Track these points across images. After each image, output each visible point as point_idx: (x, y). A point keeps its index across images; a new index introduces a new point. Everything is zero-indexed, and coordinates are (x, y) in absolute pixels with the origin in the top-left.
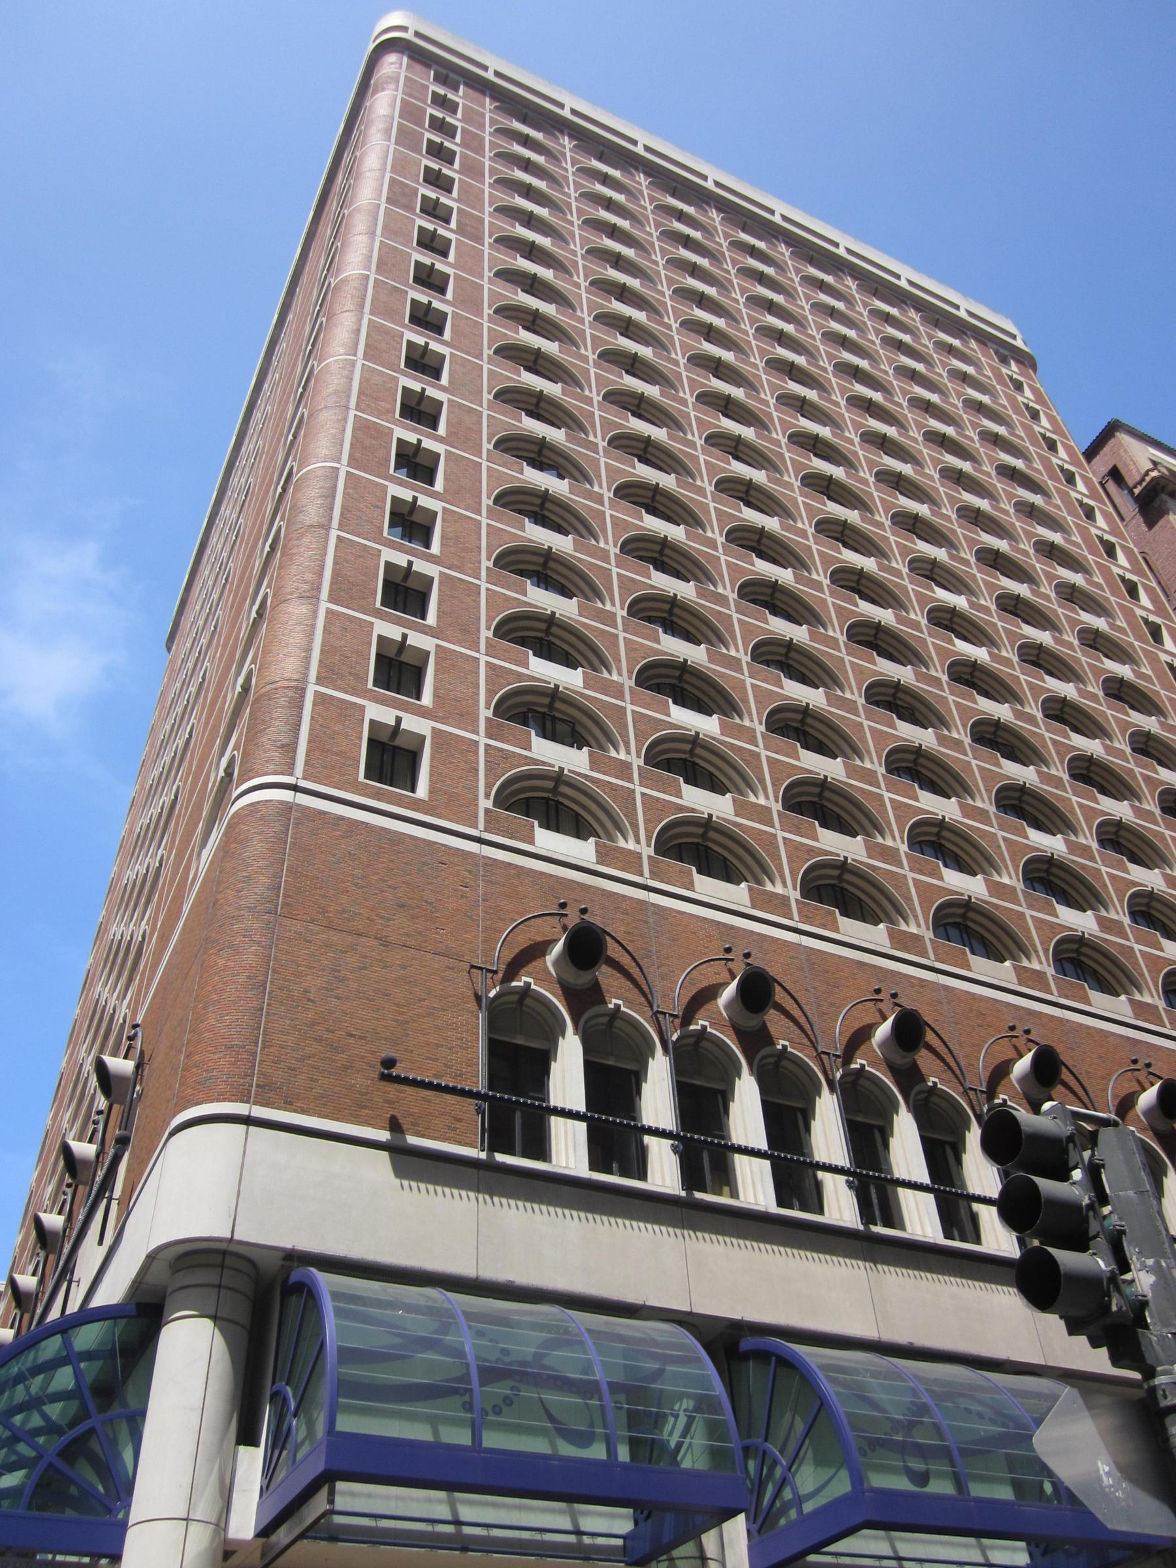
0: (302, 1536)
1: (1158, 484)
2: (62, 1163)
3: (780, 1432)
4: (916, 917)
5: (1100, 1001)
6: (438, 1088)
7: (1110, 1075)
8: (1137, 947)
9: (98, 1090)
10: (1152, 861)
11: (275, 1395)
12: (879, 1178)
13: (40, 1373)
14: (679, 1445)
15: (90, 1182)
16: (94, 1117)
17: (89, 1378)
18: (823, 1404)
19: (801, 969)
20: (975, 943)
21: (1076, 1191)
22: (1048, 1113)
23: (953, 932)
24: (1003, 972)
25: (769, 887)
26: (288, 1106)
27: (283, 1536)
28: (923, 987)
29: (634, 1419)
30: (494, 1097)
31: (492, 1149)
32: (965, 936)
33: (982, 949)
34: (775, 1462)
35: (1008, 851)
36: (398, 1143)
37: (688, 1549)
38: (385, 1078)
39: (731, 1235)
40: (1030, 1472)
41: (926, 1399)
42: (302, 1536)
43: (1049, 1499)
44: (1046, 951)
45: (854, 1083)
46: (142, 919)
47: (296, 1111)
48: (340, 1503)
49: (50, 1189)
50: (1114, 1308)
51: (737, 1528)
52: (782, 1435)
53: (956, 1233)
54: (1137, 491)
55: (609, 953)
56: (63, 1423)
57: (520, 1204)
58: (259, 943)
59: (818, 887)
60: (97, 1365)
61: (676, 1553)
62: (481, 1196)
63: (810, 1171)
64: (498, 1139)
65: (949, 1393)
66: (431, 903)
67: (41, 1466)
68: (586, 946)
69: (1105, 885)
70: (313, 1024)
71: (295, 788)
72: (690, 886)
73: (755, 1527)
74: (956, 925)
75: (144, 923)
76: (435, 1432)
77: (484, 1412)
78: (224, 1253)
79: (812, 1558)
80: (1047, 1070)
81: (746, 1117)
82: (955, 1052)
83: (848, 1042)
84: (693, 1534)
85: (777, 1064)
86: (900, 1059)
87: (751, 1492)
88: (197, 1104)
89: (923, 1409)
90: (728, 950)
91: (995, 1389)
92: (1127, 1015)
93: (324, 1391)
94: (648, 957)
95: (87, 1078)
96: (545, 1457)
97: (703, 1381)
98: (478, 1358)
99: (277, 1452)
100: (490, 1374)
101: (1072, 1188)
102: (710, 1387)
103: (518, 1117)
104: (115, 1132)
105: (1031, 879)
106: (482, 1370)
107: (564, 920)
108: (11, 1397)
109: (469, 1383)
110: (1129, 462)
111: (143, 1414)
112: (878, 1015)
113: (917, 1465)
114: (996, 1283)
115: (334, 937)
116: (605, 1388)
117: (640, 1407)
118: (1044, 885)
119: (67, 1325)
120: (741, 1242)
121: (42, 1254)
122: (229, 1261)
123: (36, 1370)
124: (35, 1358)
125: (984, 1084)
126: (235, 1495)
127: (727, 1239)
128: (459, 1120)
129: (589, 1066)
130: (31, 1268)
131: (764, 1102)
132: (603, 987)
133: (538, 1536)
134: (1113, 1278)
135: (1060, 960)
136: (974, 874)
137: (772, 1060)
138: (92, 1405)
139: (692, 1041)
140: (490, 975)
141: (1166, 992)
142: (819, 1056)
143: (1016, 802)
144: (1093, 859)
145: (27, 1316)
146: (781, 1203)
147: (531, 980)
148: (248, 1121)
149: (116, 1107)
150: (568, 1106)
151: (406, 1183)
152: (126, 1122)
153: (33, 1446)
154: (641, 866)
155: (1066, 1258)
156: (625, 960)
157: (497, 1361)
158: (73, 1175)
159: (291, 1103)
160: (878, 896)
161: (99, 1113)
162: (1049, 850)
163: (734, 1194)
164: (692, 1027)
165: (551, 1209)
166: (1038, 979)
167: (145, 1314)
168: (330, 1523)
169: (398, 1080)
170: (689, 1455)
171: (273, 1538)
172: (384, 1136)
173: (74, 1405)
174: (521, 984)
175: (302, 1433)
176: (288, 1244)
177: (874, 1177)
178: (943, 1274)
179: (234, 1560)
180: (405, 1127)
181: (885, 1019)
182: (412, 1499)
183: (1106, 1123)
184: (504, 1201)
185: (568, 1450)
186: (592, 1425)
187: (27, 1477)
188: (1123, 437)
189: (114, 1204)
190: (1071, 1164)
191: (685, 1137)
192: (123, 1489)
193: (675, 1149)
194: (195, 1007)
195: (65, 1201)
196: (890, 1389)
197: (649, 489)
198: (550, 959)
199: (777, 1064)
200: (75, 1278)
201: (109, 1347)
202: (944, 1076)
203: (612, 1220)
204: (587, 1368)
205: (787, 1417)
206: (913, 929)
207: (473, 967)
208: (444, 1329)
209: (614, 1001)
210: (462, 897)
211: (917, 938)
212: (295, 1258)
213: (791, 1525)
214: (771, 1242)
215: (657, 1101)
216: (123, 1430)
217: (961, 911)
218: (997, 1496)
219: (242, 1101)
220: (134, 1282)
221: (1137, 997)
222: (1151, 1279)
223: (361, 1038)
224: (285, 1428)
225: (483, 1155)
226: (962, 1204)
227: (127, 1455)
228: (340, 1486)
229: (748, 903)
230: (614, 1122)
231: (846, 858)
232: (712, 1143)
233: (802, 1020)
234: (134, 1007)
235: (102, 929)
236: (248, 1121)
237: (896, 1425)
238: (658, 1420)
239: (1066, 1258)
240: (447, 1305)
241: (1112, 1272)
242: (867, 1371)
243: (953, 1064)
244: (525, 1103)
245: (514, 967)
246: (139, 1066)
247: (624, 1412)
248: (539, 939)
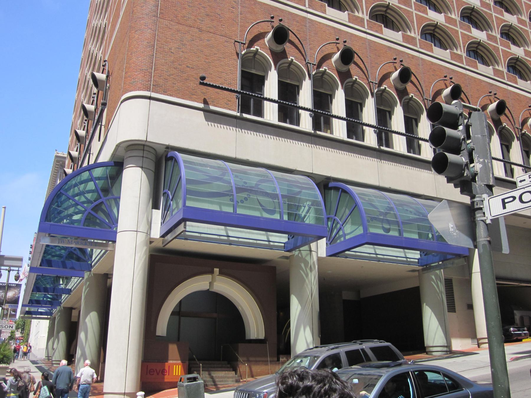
0: (175, 238)
2: (82, 112)
3: (340, 214)
4: (414, 30)
6: (222, 88)
7: (480, 97)
8: (500, 47)
9: (93, 85)
10: (514, 11)
11: (164, 194)
12: (386, 130)
13: (82, 183)
14: (305, 216)
15: (94, 118)
16: (93, 95)
17: (100, 186)
18: (356, 205)
19: (366, 48)
20: (436, 42)
21: (459, 133)
22: (454, 104)
23: (428, 37)
24: (446, 54)
25: (356, 14)
26: (165, 93)
27: (169, 237)
28: (413, 58)
29: (289, 206)
30: (243, 93)
31: (242, 112)
32: (433, 39)
33: (439, 45)
34: (338, 223)
35: (456, 4)
36: (207, 108)
37: (306, 248)
38: (202, 84)
39: (329, 147)
40: (423, 224)
41: (392, 205)
42: (175, 238)
43: (430, 239)
44: (464, 47)
45: (381, 94)
46: (104, 18)
47: (168, 95)
48: (188, 229)
49: (79, 121)
50: (465, 175)
51: (323, 242)
52: (341, 216)
53: (412, 151)
55: (290, 38)
56: (92, 200)
57: (252, 132)
58: (151, 29)
59: (376, 15)
60: (102, 181)
61: (301, 249)
62: (237, 129)
63: (361, 126)
64: (245, 108)
65: (402, 204)
66: (219, 15)
67: (86, 213)
68: (281, 35)
69: (493, 21)
70: (173, 62)
72: (324, 12)
73: (329, 243)
74: (430, 34)
75: (105, 20)
76: (220, 208)
77: (238, 202)
78: (144, 145)
79: (347, 252)
80: (456, 93)
81: (339, 105)
82: (422, 85)
83: (381, 79)
84: (307, 243)
85: (352, 85)
86: (400, 86)
87: (329, 232)
88: (131, 91)
89: (391, 209)
90: (338, 39)
91: (418, 204)
93: (181, 193)
94: (305, 40)
95: (89, 81)
96: (258, 217)
97: (316, 196)
98: (235, 184)
99: (166, 212)
100: (240, 190)
101: (459, 133)
102: (317, 198)
103: (252, 100)
104: (101, 101)
105: (464, 17)
106: (237, 188)
107: (272, 24)
108: (74, 191)
109: (232, 192)
111: (119, 198)
112: (394, 68)
113: (387, 226)
114: (424, 169)
115: (181, 27)
116: (280, 197)
117: (292, 204)
118: (468, 19)
119: (90, 168)
120: (333, 150)
121: (79, 144)
122: (146, 148)
123: (82, 183)
124: (80, 179)
125: (431, 97)
126: (152, 225)
127: (328, 149)
128: (230, 101)
129: (280, 83)
130: (75, 149)
132: (287, 52)
133: (255, 242)
134: (467, 165)
135: (469, 51)
136: (440, 13)
137: (351, 84)
138: (102, 194)
139: (320, 74)
140: (242, 45)
141: (508, 66)
142: (369, 83)
144: (490, 10)
145: (76, 165)
146: (349, 137)
147: (259, 48)
148: (150, 98)
149: (100, 92)
150: (271, 98)
151: (210, 123)
152: (105, 97)
153: (83, 207)
154: (305, 2)
155: (451, 157)
156: (296, 41)
157: (242, 186)
158: (87, 116)
159: (166, 92)
161: (94, 94)
162: (473, 5)
163: (332, 133)
164: (321, 69)
165: (263, 135)
166: (459, 58)
167: (117, 166)
168: (185, 234)
169: (206, 85)
170: (308, 219)
171: (166, 238)
172: (201, 106)
173: (95, 195)
174: (255, 49)
175: (174, 206)
176: (167, 143)
177: (384, 129)
178: (405, 165)
179: (153, 244)
180: (209, 103)
181: (396, 70)
182: (213, 229)
183: (475, 110)
184: (246, 131)
185: (266, 215)
186: (275, 208)
187: (82, 216)
189: (103, 127)
190: (459, 124)
191: (315, 111)
192: (115, 221)
193: (311, 115)
194: (128, 54)
195: (85, 126)
196: (381, 201)
198: (266, 39)
199: (352, 85)
200: (91, 153)
201: (106, 176)
202: (416, 94)
203: (286, 140)
204: (275, 190)
205: (344, 208)
206: (413, 35)
207: (236, 41)
208: (224, 174)
209: (291, 57)
210: (232, 12)
211: (414, 39)
212: (169, 148)
213: (341, 242)
214: (344, 151)
215: (305, 97)
216: (113, 203)
217: (433, 28)
218: (412, 237)
219: (147, 91)
220: (112, 154)
221: (497, 67)
222: (481, 166)
223: (192, 68)
224: (168, 204)
225: (238, 114)
226: (416, 140)
227: (115, 211)
228: (188, 223)
229: (347, 20)
230: (288, 104)
231: (389, 3)
232: (325, 114)
233: (364, 69)
234: (104, 54)
235: (89, 22)
236: (150, 98)
237: (381, 213)
238: (298, 208)
239: (451, 157)
240: (225, 166)
241: (467, 162)
242: (373, 196)
243: (420, 89)
244: (255, 96)
245: (252, 43)
246: (107, 77)
247: (287, 205)
248: (262, 31)
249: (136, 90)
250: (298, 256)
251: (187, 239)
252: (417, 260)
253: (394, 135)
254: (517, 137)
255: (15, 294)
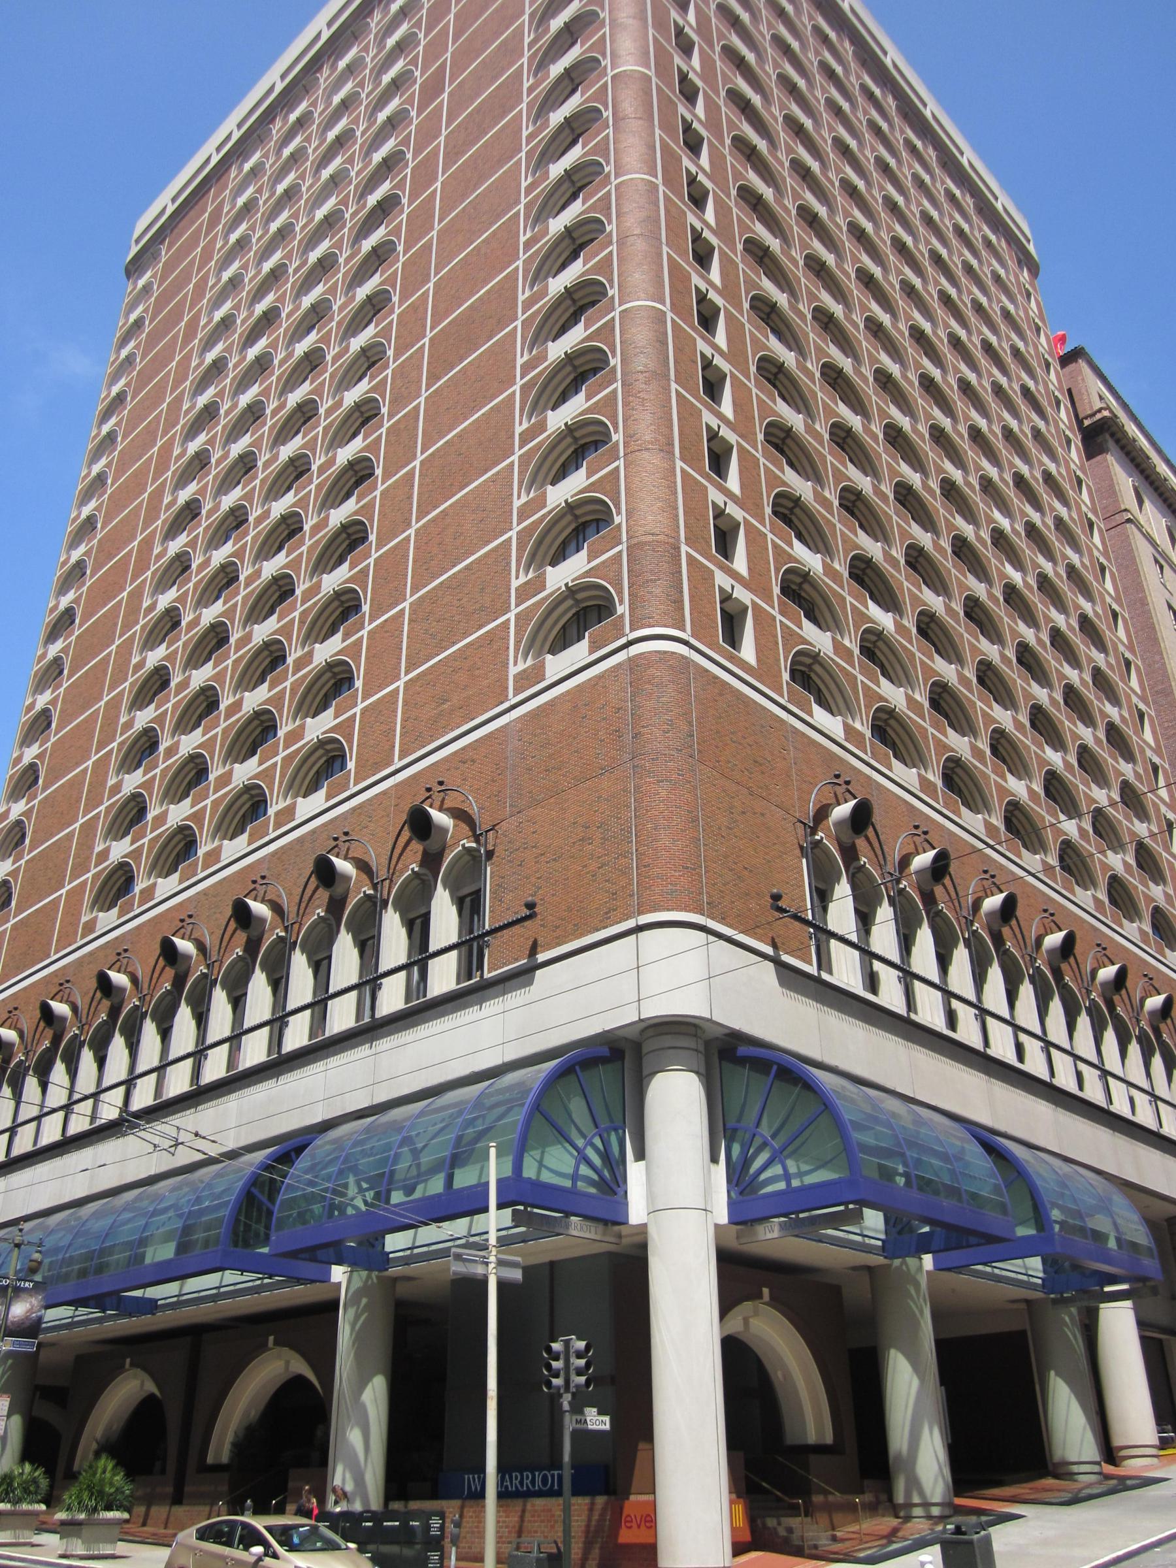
1: (1105, 423)
5: (820, 716)
54: (1087, 423)
71: (686, 643)
88: (668, 910)
92: (981, 831)
110: (1083, 391)
112: (912, 846)
131: (937, 952)
143: (787, 512)
160: (908, 742)
188: (1082, 364)
197: (767, 304)
248: (825, 802)
249: (681, 910)
250: (899, 1268)
251: (820, 1241)
252: (879, 1243)
253: (833, 941)
254: (889, 896)
255: (30, 1311)
